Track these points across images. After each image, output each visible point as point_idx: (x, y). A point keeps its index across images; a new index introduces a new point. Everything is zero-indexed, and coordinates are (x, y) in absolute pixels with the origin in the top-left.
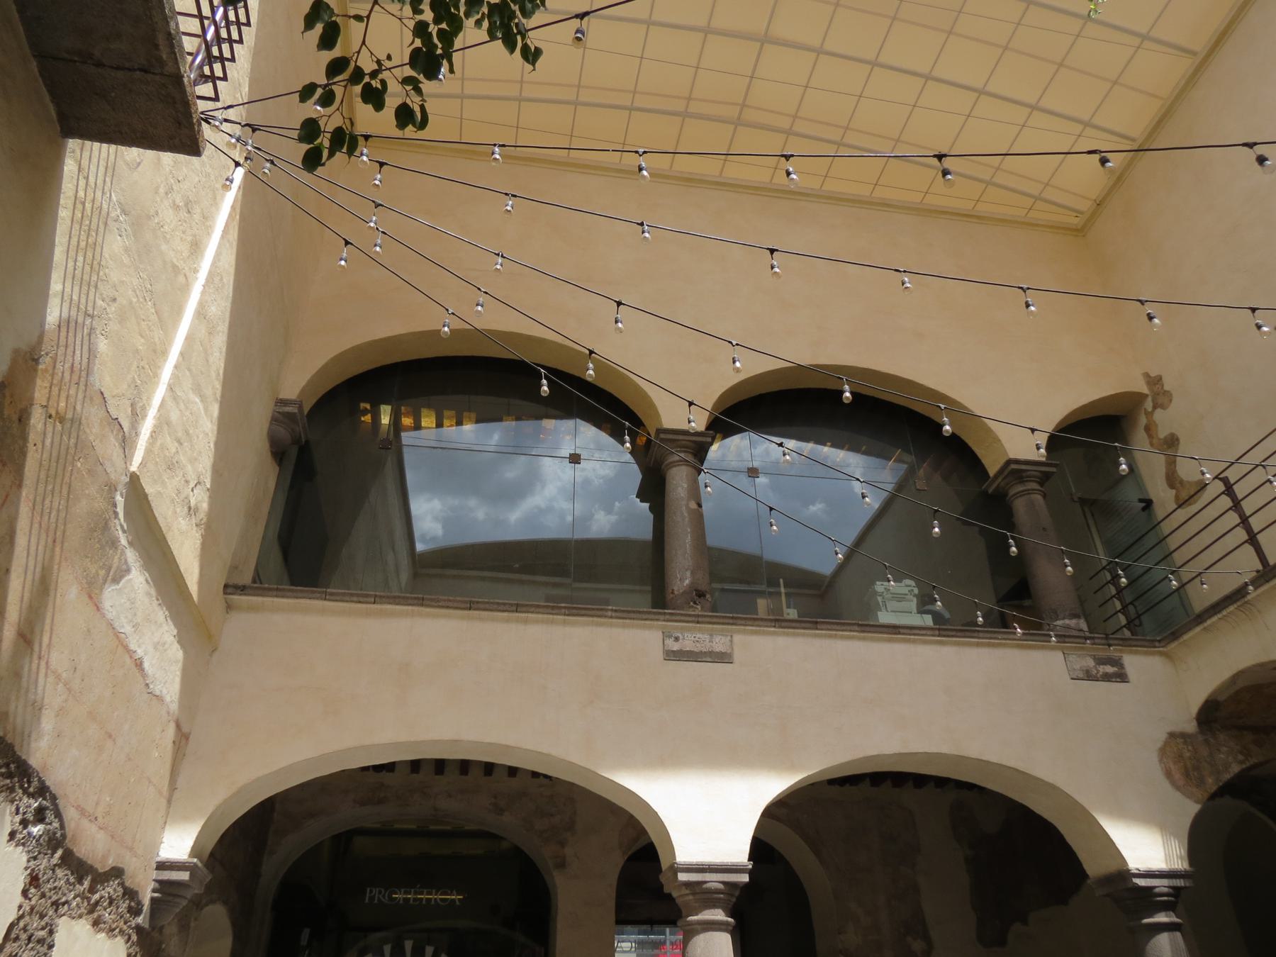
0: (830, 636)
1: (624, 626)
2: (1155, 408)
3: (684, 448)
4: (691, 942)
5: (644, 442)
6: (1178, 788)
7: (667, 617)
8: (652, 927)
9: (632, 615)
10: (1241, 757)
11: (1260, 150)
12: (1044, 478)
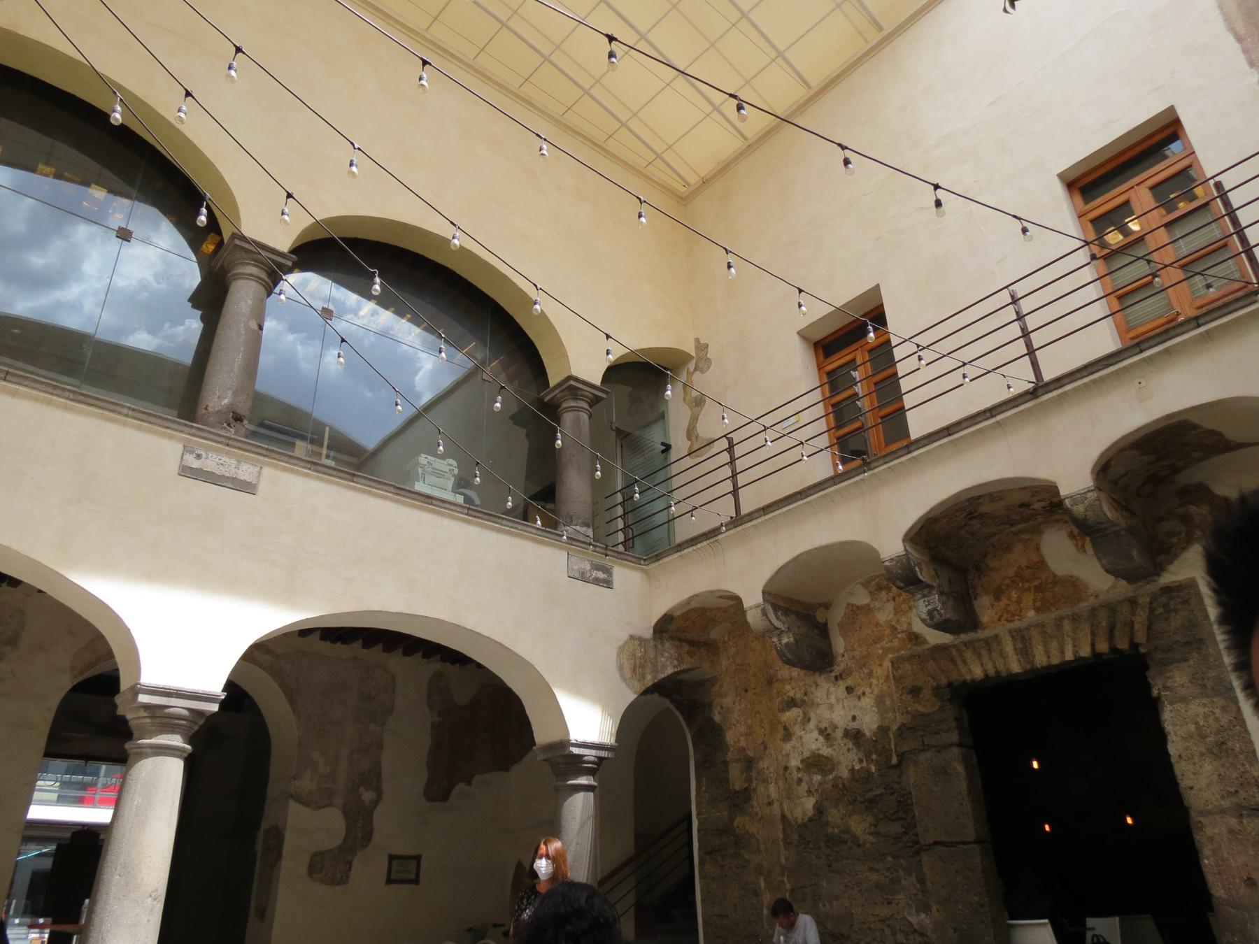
0: (364, 492)
1: (139, 428)
2: (696, 370)
3: (260, 263)
4: (136, 765)
5: (211, 250)
6: (624, 680)
7: (194, 431)
8: (86, 763)
9: (153, 419)
10: (676, 662)
11: (848, 153)
12: (595, 401)
